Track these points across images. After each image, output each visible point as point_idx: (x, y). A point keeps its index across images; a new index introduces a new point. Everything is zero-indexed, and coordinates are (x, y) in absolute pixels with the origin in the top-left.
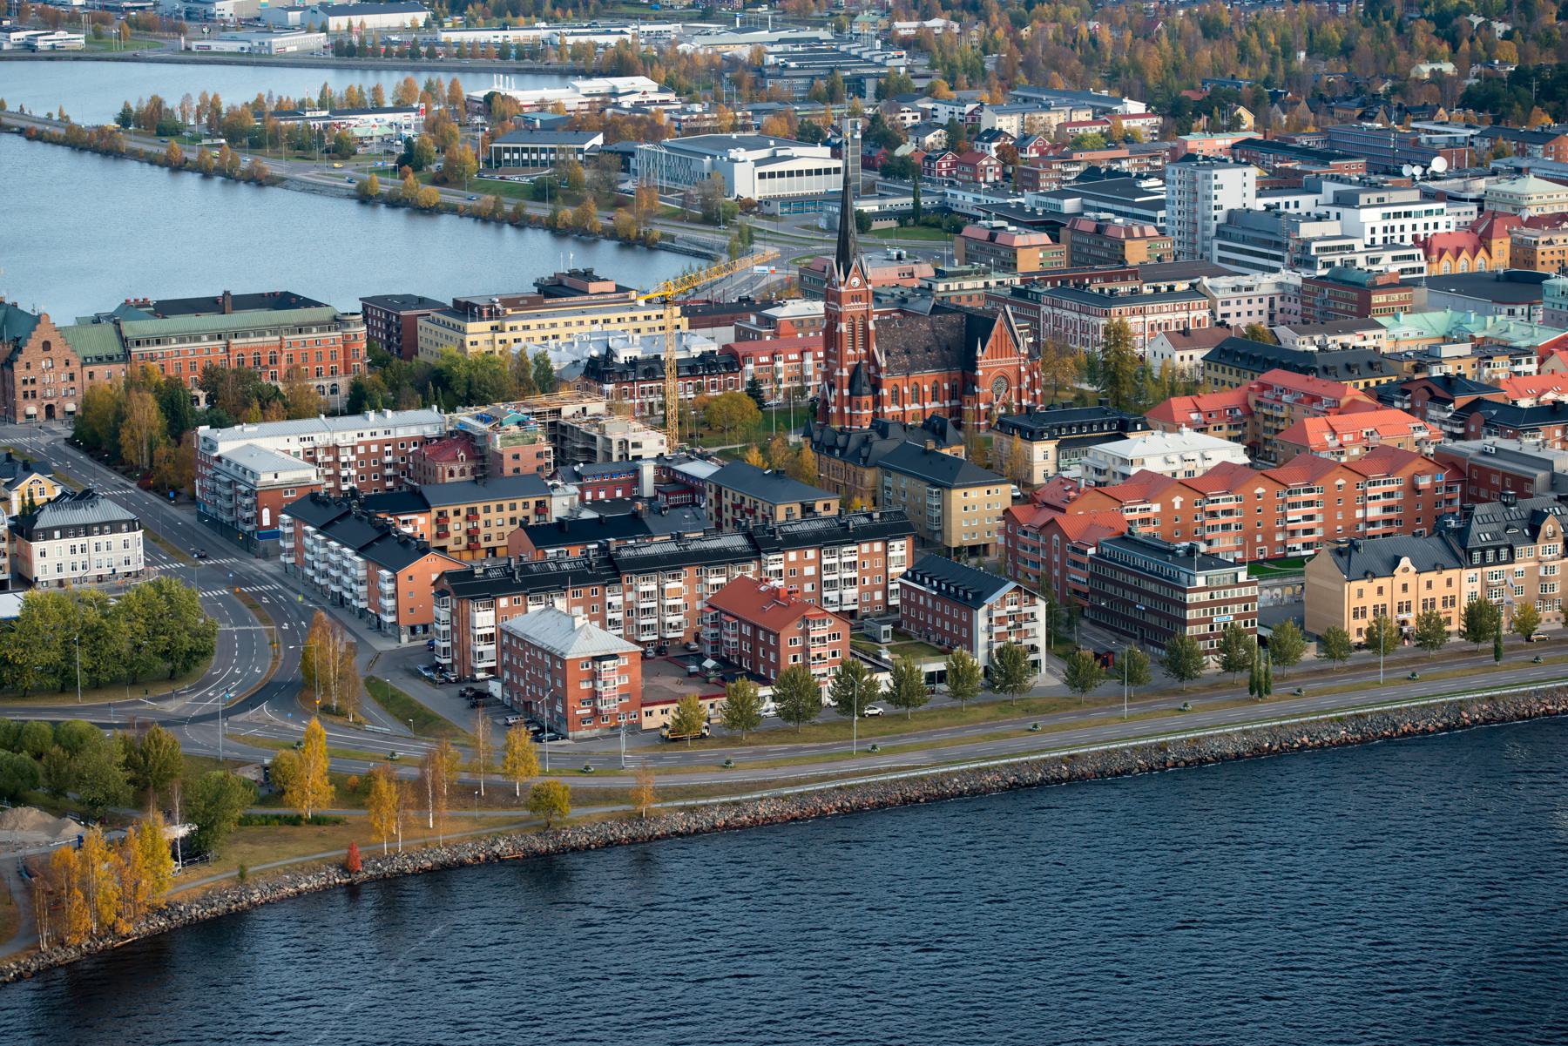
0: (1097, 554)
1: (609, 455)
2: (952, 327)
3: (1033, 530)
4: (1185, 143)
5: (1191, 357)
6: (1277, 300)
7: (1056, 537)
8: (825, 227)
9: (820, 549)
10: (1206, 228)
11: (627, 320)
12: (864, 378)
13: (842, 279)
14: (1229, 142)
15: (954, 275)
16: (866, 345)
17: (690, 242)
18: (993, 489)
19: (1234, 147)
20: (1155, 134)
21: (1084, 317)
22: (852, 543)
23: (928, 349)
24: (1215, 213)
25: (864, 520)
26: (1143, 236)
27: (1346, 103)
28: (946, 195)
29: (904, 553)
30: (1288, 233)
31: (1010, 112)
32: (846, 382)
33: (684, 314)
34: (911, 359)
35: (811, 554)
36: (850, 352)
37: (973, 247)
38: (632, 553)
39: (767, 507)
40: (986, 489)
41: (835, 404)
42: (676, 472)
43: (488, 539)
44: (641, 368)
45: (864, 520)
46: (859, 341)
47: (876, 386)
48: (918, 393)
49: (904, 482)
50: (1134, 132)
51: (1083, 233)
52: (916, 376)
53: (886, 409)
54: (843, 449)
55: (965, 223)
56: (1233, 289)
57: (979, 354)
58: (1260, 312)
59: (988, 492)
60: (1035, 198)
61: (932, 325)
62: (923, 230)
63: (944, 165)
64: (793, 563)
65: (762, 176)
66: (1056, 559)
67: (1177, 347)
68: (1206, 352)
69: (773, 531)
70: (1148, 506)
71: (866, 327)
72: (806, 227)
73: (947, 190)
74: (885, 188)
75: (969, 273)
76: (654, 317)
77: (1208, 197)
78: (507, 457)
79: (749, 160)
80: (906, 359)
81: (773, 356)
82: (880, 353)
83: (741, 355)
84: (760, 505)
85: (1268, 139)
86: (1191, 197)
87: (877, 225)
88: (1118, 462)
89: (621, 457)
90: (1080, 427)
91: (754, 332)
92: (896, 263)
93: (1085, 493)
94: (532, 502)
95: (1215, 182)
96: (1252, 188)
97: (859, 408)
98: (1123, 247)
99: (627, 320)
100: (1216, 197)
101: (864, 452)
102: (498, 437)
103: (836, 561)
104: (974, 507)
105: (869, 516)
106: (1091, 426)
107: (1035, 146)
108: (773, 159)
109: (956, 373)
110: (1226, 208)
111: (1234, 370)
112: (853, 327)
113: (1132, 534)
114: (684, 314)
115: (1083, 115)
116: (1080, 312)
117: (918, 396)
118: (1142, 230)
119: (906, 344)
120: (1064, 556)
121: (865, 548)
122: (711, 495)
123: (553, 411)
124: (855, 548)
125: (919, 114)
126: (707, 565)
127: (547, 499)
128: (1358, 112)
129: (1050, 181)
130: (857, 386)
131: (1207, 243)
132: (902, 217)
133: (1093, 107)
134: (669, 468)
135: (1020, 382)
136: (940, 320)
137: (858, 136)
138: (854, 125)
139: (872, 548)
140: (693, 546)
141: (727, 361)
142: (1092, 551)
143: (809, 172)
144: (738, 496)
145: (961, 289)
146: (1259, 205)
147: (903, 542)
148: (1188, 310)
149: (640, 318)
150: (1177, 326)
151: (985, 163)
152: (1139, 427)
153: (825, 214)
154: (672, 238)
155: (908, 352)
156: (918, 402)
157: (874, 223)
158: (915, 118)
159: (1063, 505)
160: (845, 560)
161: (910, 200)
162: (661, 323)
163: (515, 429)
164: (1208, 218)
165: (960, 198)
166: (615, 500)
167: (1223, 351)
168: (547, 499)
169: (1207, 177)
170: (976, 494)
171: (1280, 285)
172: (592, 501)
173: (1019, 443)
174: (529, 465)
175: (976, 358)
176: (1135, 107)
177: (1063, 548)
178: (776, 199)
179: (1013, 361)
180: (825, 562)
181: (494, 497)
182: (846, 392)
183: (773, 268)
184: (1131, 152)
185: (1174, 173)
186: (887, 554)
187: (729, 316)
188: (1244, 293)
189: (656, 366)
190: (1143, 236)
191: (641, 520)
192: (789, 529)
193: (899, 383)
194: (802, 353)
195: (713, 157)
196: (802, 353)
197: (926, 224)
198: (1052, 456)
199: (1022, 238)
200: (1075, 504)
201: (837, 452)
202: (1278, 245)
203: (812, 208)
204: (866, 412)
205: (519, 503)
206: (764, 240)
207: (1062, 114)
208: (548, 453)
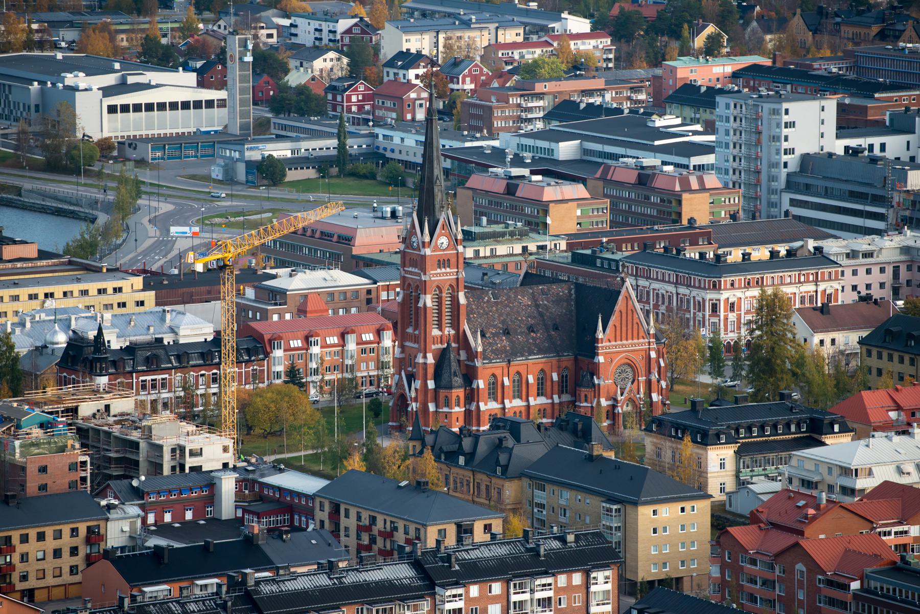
0: (862, 589)
1: (158, 467)
2: (558, 301)
3: (765, 559)
4: (674, 70)
5: (833, 341)
6: (903, 269)
7: (800, 567)
8: (220, 178)
9: (508, 582)
10: (772, 178)
11: (76, 294)
12: (454, 366)
13: (427, 239)
14: (729, 70)
15: (484, 237)
16: (455, 324)
17: (44, 195)
18: (688, 505)
19: (735, 75)
20: (609, 60)
21: (683, 290)
22: (546, 573)
23: (531, 329)
24: (785, 158)
25: (556, 544)
26: (703, 189)
27: (857, 19)
28: (377, 136)
29: (609, 587)
30: (893, 184)
31: (421, 30)
32: (431, 371)
33: (146, 287)
34: (511, 342)
35: (497, 588)
36: (436, 332)
37: (484, 202)
38: (274, 588)
39: (412, 528)
40: (679, 506)
41: (416, 400)
42: (263, 485)
43: (24, 578)
44: (141, 355)
45: (556, 544)
46: (446, 319)
47: (469, 376)
48: (520, 386)
49: (566, 497)
50: (587, 55)
51: (620, 184)
52: (519, 363)
53: (483, 407)
54: (470, 457)
55: (470, 173)
56: (848, 255)
57: (600, 335)
58: (882, 285)
59: (683, 510)
60: (517, 140)
61: (534, 298)
62: (351, 182)
63: (354, 99)
64: (474, 599)
65: (112, 109)
66: (801, 596)
67: (815, 329)
68: (865, 334)
69: (448, 558)
70: (906, 528)
71: (455, 300)
72: (193, 177)
73: (377, 130)
74: (284, 127)
75: (503, 235)
76: (110, 291)
77: (776, 138)
78: (32, 469)
79: (95, 88)
80: (504, 342)
81: (307, 340)
82: (474, 334)
83: (266, 337)
84: (400, 525)
85: (779, 65)
86: (754, 138)
87: (292, 175)
88: (836, 472)
89: (173, 468)
90: (762, 428)
91: (255, 310)
92: (389, 222)
93: (827, 510)
94: (83, 528)
95: (786, 118)
96: (831, 126)
97: (448, 404)
98: (680, 202)
99: (76, 294)
100: (786, 139)
101: (503, 458)
102: (17, 443)
103: (526, 597)
104: (665, 530)
105: (562, 539)
106: (775, 427)
107: (470, 75)
108: (122, 87)
109: (567, 359)
110: (798, 153)
111: (907, 358)
112: (439, 301)
113: (908, 563)
114: (146, 287)
115: (511, 35)
116: (676, 284)
117: (520, 390)
118: (701, 180)
119: (503, 322)
120: (813, 591)
121: (562, 580)
122: (323, 515)
123: (67, 410)
124: (550, 580)
125: (274, 32)
126: (371, 603)
127: (102, 524)
128: (875, 29)
129: (506, 119)
130: (445, 376)
131: (774, 198)
132: (322, 164)
133: (525, 25)
134: (254, 481)
135: (649, 372)
136: (543, 292)
137: (249, 58)
138: (244, 44)
139: (570, 580)
140: (351, 579)
141: (251, 346)
142: (855, 585)
143: (174, 106)
144: (365, 515)
145: (493, 255)
146: (838, 147)
147: (608, 573)
148: (816, 282)
149: (93, 291)
150: (802, 302)
151: (413, 95)
152: (836, 428)
153: (221, 162)
154: (18, 191)
155: (507, 332)
156: (496, 400)
157: (288, 173)
158: (270, 36)
159: (798, 527)
160: (539, 595)
161: (334, 142)
162: (119, 298)
163: (37, 433)
164: (776, 165)
165: (397, 140)
166: (185, 524)
167: (888, 332)
168: (102, 524)
169: (776, 112)
170: (668, 512)
171: (906, 250)
172: (155, 525)
173: (688, 447)
174: (59, 480)
175: (596, 340)
176: (578, 24)
177: (811, 581)
178: (147, 140)
179: (641, 344)
180: (514, 598)
181: (32, 523)
182: (431, 384)
183: (197, 229)
184: (607, 83)
185: (728, 106)
186: (588, 588)
187: (204, 289)
188: (861, 260)
189: (161, 352)
190: (703, 189)
191: (258, 546)
192: (465, 555)
193: (498, 372)
194: (343, 336)
195: (42, 83)
196: (343, 336)
197: (354, 174)
198: (730, 466)
199: (552, 191)
200: (816, 525)
201: (462, 460)
202: (878, 200)
203: (192, 153)
204: (457, 409)
205: (66, 529)
206: (158, 194)
207: (486, 33)
208: (84, 463)
